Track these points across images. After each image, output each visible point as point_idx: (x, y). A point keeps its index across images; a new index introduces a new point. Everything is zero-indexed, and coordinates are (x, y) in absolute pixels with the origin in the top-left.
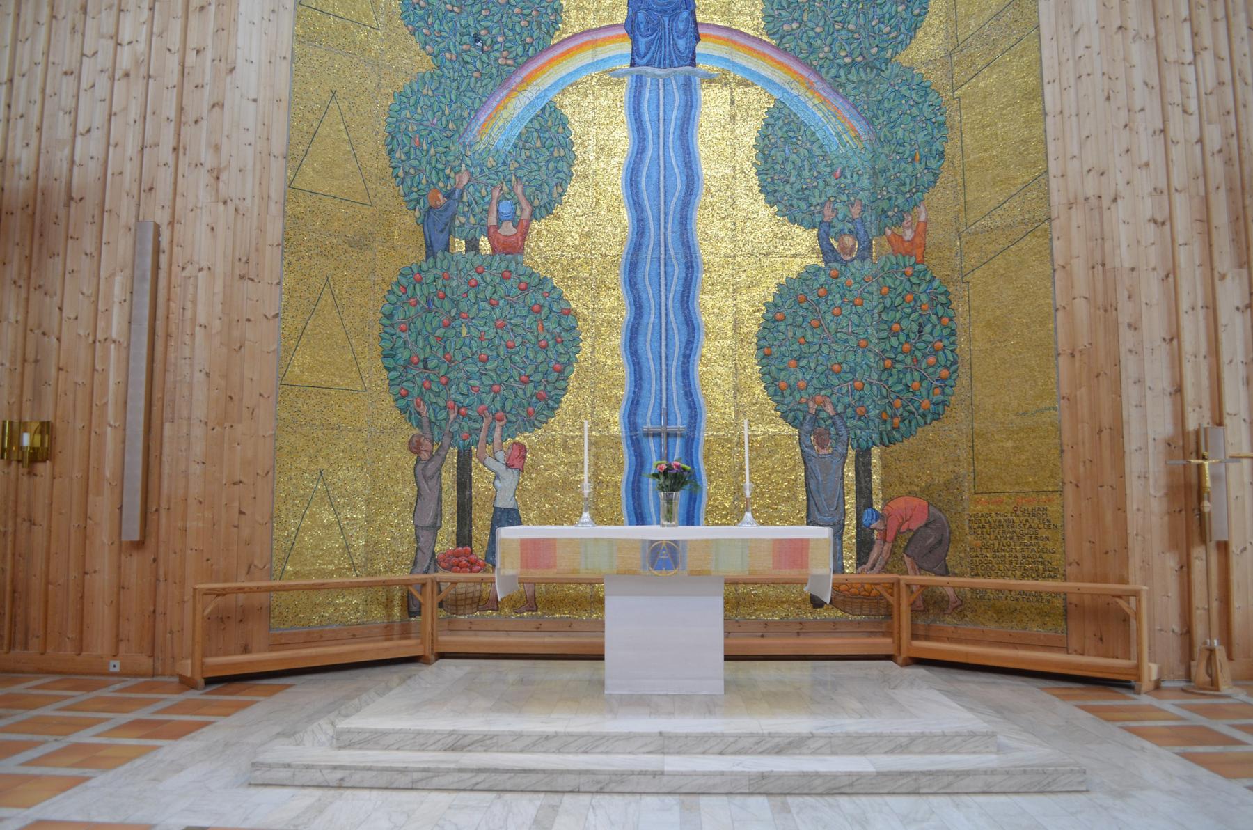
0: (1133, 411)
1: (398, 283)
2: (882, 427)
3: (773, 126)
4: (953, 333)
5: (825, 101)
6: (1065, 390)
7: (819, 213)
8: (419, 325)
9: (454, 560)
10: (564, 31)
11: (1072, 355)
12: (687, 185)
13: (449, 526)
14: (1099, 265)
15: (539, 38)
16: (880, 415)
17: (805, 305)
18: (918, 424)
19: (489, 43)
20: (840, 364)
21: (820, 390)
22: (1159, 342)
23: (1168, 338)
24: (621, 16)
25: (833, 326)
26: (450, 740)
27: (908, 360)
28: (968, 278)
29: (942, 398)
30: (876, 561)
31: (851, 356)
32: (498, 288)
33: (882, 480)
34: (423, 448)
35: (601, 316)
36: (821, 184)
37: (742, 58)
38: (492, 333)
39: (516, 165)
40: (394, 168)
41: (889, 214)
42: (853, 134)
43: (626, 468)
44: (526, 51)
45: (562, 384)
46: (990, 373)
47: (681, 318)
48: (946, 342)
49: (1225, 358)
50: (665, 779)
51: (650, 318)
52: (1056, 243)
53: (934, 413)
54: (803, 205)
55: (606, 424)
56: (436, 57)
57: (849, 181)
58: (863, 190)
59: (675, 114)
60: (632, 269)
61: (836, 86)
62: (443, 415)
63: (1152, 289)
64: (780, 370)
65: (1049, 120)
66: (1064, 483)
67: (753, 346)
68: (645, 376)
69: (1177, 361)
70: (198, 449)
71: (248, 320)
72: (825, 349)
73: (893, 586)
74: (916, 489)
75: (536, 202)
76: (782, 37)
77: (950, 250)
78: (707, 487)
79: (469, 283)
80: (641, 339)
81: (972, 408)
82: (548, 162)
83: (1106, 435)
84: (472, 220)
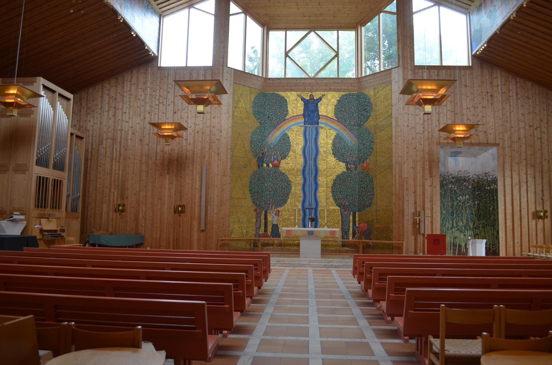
0: (406, 207)
13: (263, 228)
14: (400, 176)
24: (302, 112)
37: (329, 123)
41: (361, 160)
51: (308, 182)
59: (314, 136)
60: (304, 171)
61: (350, 130)
63: (411, 182)
69: (415, 197)
70: (215, 211)
73: (359, 242)
78: (320, 220)
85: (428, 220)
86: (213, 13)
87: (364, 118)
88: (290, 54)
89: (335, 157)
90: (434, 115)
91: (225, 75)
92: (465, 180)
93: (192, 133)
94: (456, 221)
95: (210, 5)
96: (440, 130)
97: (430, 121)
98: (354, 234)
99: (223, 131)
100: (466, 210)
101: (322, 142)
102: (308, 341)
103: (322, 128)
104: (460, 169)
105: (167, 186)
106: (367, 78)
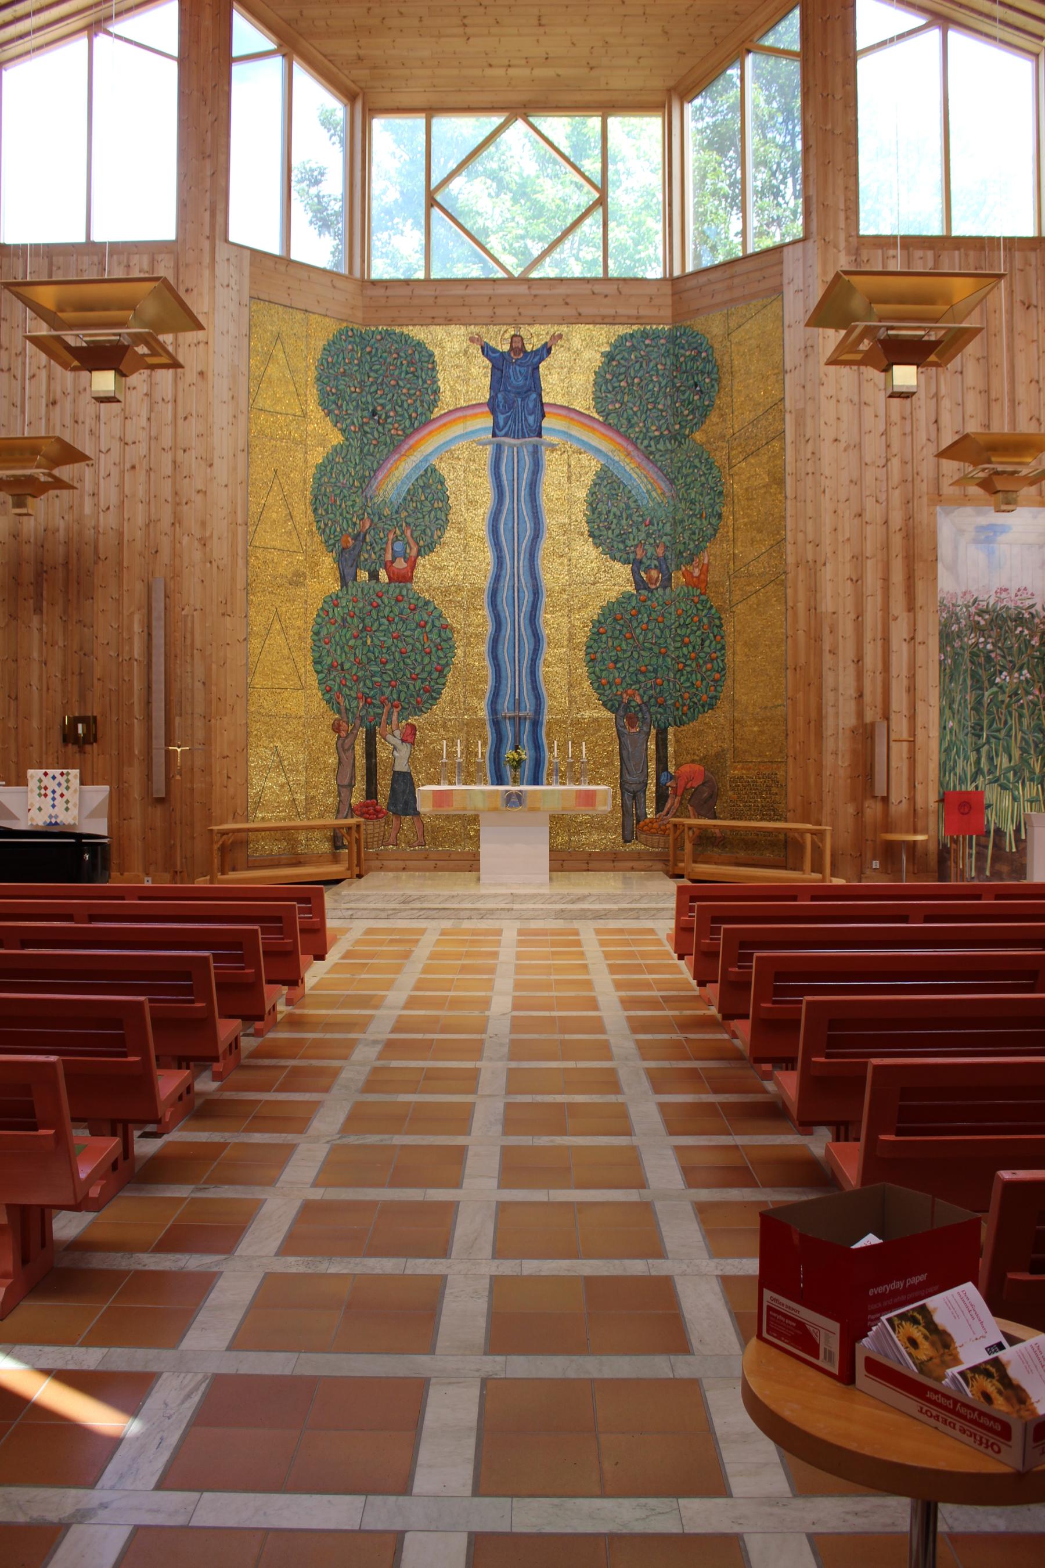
1: (322, 609)
2: (676, 713)
3: (600, 485)
4: (723, 648)
5: (639, 466)
6: (790, 694)
9: (365, 809)
10: (442, 408)
11: (795, 669)
13: (360, 785)
14: (813, 608)
15: (421, 414)
16: (674, 704)
17: (621, 622)
18: (699, 712)
19: (383, 416)
22: (850, 663)
24: (485, 396)
25: (641, 638)
26: (402, 899)
27: (694, 665)
28: (734, 609)
30: (669, 809)
31: (654, 661)
34: (342, 728)
35: (471, 630)
36: (635, 530)
37: (576, 431)
39: (406, 514)
42: (659, 492)
43: (489, 742)
44: (412, 424)
47: (529, 631)
48: (719, 654)
49: (894, 672)
51: (507, 631)
52: (789, 591)
54: (621, 546)
58: (666, 535)
59: (526, 476)
62: (354, 704)
63: (846, 626)
65: (789, 502)
68: (503, 674)
72: (636, 655)
74: (696, 758)
75: (421, 543)
76: (608, 414)
80: (500, 647)
81: (734, 703)
82: (430, 512)
85: (900, 752)
86: (175, 52)
87: (692, 412)
88: (438, 198)
89: (596, 545)
90: (922, 402)
91: (221, 268)
92: (1019, 620)
93: (115, 472)
94: (989, 752)
95: (161, 25)
96: (942, 454)
97: (908, 422)
98: (661, 798)
99: (216, 461)
100: (1021, 716)
101: (555, 494)
102: (443, 1278)
103: (553, 447)
104: (1004, 584)
105: (35, 655)
106: (702, 279)
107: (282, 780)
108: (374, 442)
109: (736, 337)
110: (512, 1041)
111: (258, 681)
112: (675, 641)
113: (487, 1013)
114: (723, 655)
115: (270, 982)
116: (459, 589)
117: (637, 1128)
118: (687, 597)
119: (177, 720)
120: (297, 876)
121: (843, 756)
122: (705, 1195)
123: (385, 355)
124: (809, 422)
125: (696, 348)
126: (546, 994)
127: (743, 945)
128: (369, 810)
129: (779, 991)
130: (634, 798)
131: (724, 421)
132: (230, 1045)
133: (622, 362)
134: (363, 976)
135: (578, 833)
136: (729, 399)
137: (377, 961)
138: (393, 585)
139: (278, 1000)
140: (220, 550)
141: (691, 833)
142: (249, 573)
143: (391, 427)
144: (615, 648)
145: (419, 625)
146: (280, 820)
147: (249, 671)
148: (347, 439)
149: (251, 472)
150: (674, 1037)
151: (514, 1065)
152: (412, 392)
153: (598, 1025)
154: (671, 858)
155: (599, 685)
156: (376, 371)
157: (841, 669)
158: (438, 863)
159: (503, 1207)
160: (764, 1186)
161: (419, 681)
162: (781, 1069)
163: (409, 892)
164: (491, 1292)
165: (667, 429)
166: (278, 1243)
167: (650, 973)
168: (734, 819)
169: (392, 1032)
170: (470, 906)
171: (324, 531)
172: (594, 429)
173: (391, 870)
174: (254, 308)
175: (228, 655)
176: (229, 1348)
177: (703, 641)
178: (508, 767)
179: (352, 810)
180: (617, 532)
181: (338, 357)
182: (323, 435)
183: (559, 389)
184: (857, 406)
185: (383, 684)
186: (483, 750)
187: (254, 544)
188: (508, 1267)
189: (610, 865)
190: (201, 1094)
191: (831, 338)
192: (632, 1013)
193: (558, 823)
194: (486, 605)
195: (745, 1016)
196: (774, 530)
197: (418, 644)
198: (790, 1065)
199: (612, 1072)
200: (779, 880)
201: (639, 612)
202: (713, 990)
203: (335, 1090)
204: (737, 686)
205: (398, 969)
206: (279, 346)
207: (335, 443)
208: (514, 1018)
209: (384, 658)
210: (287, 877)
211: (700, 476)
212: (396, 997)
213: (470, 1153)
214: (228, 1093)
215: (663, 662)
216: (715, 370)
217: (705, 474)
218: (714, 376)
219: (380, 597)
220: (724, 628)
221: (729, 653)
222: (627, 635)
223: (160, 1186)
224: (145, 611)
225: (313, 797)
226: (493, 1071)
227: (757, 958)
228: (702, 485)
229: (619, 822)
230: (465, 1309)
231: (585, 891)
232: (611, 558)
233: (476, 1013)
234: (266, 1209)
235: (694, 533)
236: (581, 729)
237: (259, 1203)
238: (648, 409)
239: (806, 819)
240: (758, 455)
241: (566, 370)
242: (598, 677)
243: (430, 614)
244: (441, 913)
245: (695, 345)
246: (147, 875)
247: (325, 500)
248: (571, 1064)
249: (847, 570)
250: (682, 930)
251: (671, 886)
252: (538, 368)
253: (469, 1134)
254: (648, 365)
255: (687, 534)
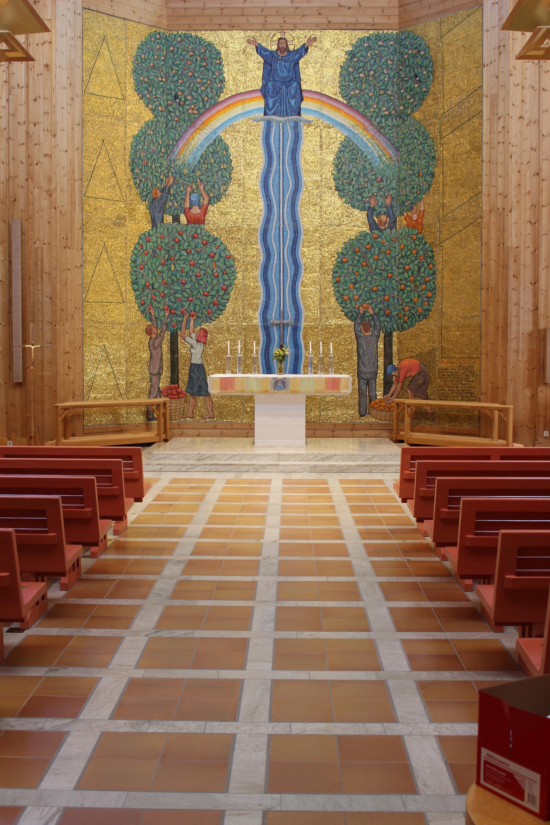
1: (138, 243)
2: (399, 321)
4: (434, 273)
5: (373, 137)
6: (484, 307)
7: (368, 202)
8: (149, 265)
9: (170, 391)
11: (488, 289)
12: (296, 184)
13: (166, 374)
14: (501, 244)
16: (397, 315)
17: (359, 254)
18: (416, 321)
19: (183, 100)
20: (377, 286)
21: (366, 301)
22: (528, 284)
23: (533, 283)
24: (259, 84)
25: (374, 265)
26: (198, 457)
27: (412, 286)
28: (442, 244)
29: (428, 307)
30: (394, 392)
32: (191, 243)
33: (398, 350)
34: (152, 332)
35: (248, 259)
37: (327, 111)
38: (188, 268)
39: (200, 173)
40: (134, 179)
42: (388, 157)
45: (226, 297)
46: (451, 296)
48: (431, 278)
50: (279, 467)
51: (275, 260)
53: (424, 315)
54: (359, 197)
55: (251, 319)
56: (154, 110)
57: (385, 184)
58: (393, 189)
59: (289, 145)
61: (380, 129)
62: (162, 314)
63: (526, 257)
64: (344, 290)
65: (484, 165)
66: (481, 354)
67: (330, 277)
71: (69, 269)
72: (369, 278)
74: (414, 354)
75: (211, 195)
76: (350, 99)
77: (435, 228)
79: (174, 240)
80: (269, 272)
81: (442, 314)
82: (218, 171)
83: (500, 330)
84: (176, 204)
89: (341, 197)
98: (387, 384)
99: (59, 133)
101: (311, 158)
103: (309, 123)
107: (109, 370)
108: (176, 119)
109: (447, 39)
110: (281, 562)
111: (91, 297)
112: (398, 268)
113: (261, 541)
114: (434, 279)
115: (102, 518)
116: (239, 229)
117: (374, 626)
118: (408, 235)
119: (31, 325)
120: (120, 440)
121: (523, 354)
122: (425, 676)
123: (184, 53)
124: (501, 103)
125: (416, 48)
126: (304, 527)
127: (452, 492)
128: (173, 392)
129: (479, 526)
130: (367, 384)
131: (437, 103)
132: (74, 565)
133: (361, 58)
134: (170, 514)
135: (327, 410)
136: (441, 87)
137: (180, 503)
138: (190, 225)
139: (108, 531)
140: (62, 199)
141: (409, 409)
142: (84, 217)
143: (188, 107)
144: (354, 273)
145: (209, 256)
146: (108, 399)
147: (84, 289)
148: (156, 117)
149: (85, 140)
150: (399, 559)
151: (282, 579)
152: (204, 81)
153: (343, 551)
154: (394, 428)
155: (342, 300)
156: (177, 65)
157: (522, 289)
158: (224, 431)
159: (276, 683)
160: (468, 670)
161: (210, 297)
162: (480, 583)
163: (202, 452)
164: (269, 746)
165: (394, 109)
166: (110, 710)
167: (380, 512)
168: (441, 399)
169: (192, 554)
170: (247, 462)
171: (139, 186)
172: (340, 110)
173: (189, 436)
174: (86, 16)
175: (69, 278)
176: (77, 788)
177: (419, 268)
178: (275, 361)
179: (160, 392)
180: (356, 187)
181: (149, 54)
182: (138, 114)
183: (314, 79)
184: (537, 91)
185: (183, 299)
186: (257, 349)
187: (87, 195)
188: (281, 728)
189: (350, 433)
190: (53, 600)
191: (520, 39)
192: (368, 542)
193: (311, 401)
194: (259, 241)
195: (455, 545)
196: (473, 185)
197: (209, 270)
198: (486, 581)
199: (354, 584)
200: (475, 444)
201: (372, 246)
202: (429, 525)
203: (151, 598)
204: (444, 301)
205: (195, 509)
206: (105, 46)
207: (147, 119)
208: (281, 544)
209: (181, 282)
210: (112, 441)
211: (419, 145)
212: (195, 529)
213: (251, 644)
214: (72, 599)
215: (389, 282)
216: (431, 65)
217: (422, 144)
218: (430, 69)
219: (181, 235)
220: (435, 259)
221: (439, 277)
222: (363, 264)
223: (23, 668)
224: (6, 244)
225: (132, 383)
226: (267, 583)
227: (464, 501)
228: (420, 152)
229: (356, 401)
230: (250, 759)
231: (331, 452)
232: (352, 206)
233: (254, 541)
234: (101, 684)
235: (413, 188)
236: (329, 333)
237: (96, 681)
238: (380, 94)
239: (494, 401)
240: (462, 129)
241: (319, 65)
242: (341, 295)
243: (217, 248)
244: (226, 468)
245: (415, 46)
246: (10, 439)
247: (140, 162)
248: (323, 579)
249: (528, 215)
250: (406, 482)
251: (396, 450)
252: (298, 63)
253: (250, 630)
254: (380, 61)
255: (408, 188)
